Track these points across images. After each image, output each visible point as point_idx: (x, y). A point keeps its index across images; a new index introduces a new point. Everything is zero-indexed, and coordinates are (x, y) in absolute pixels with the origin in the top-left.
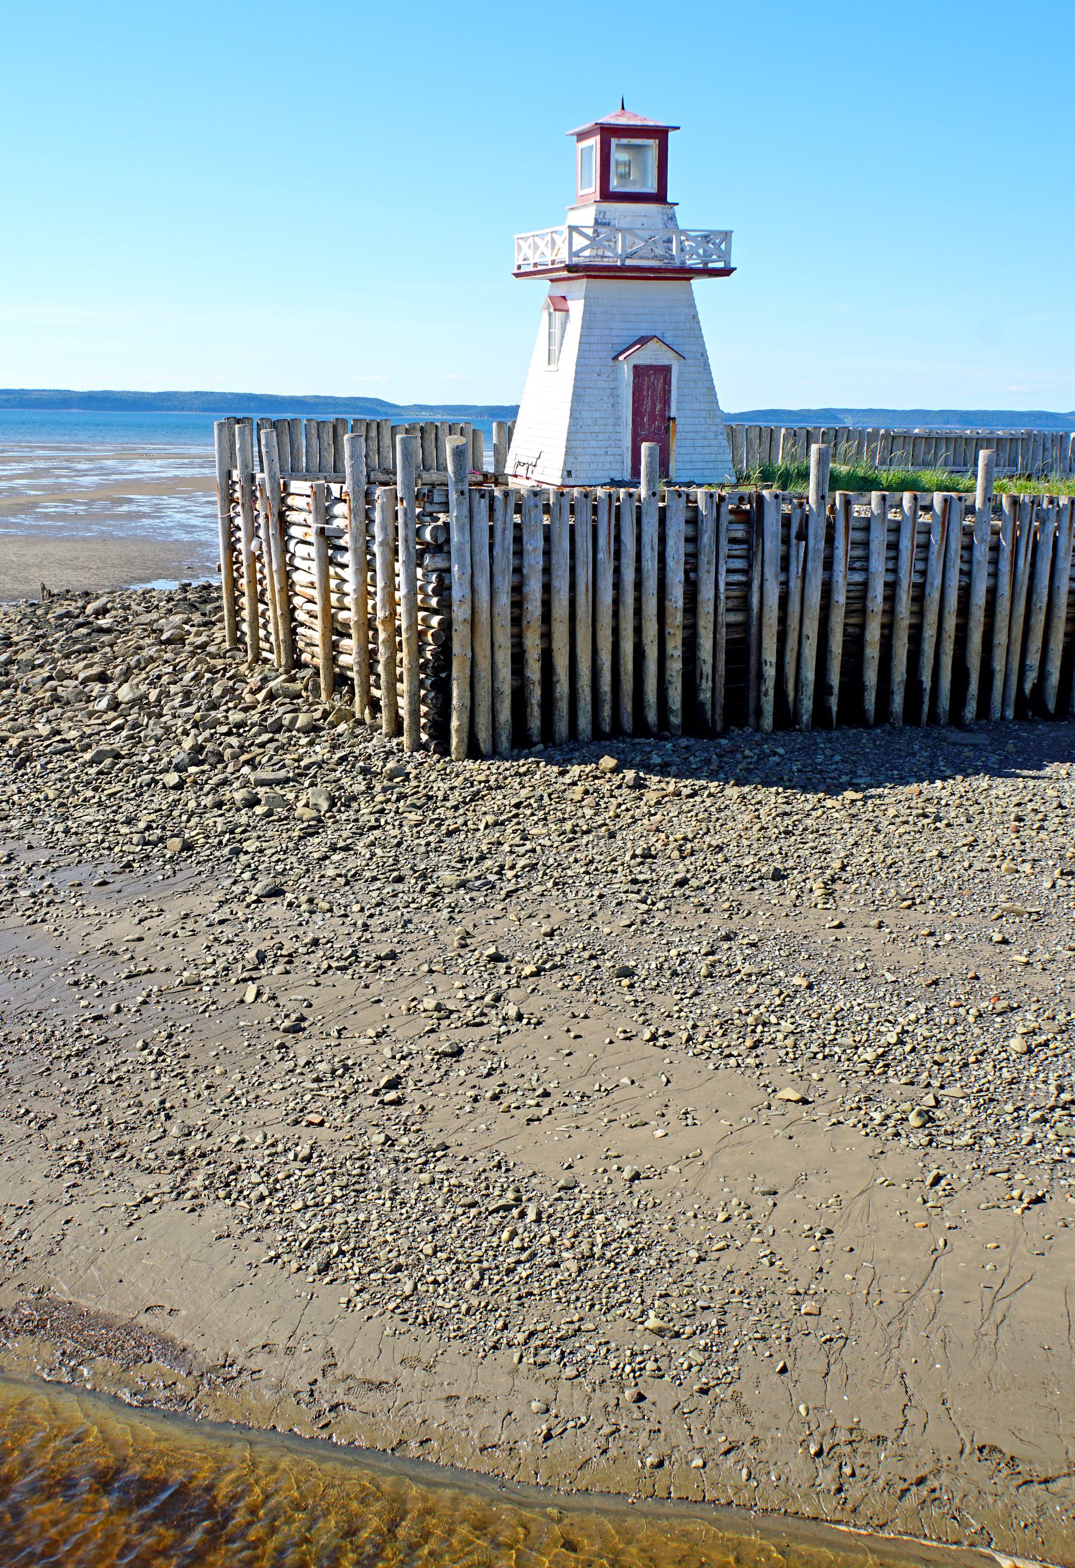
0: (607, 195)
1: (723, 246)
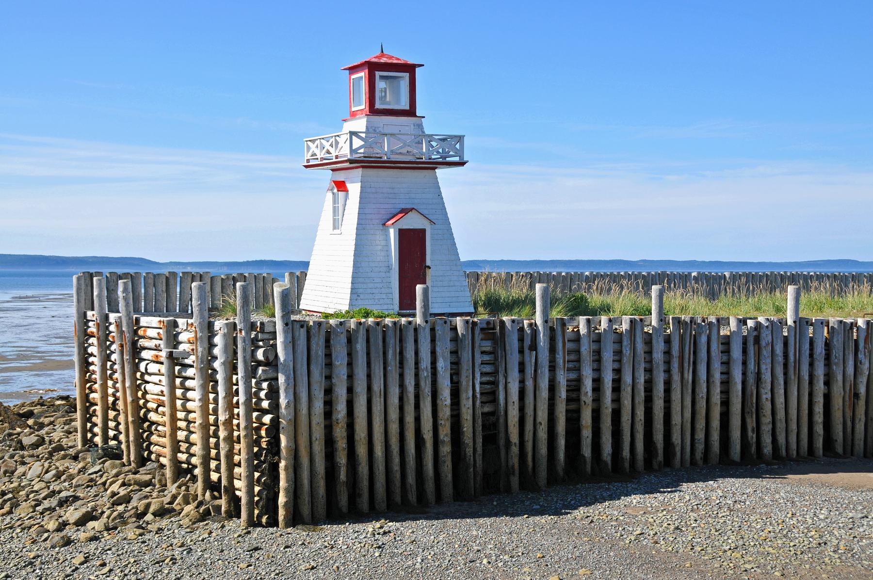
0: (373, 111)
1: (458, 146)
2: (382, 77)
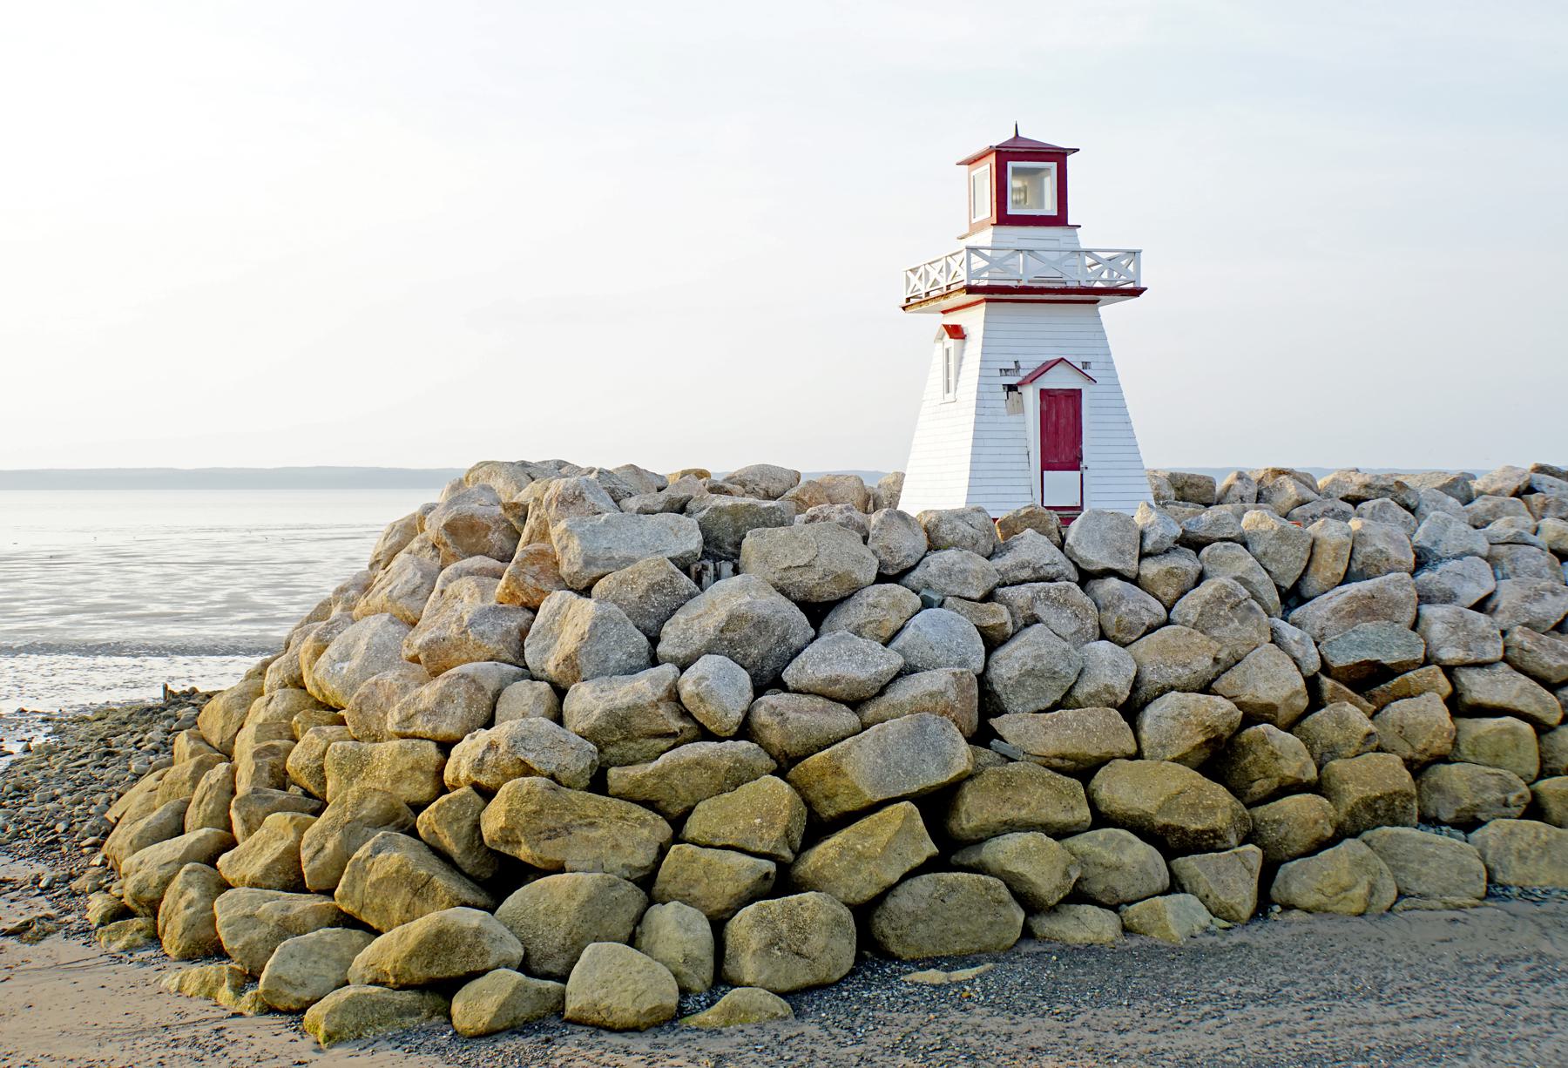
2: (1016, 171)
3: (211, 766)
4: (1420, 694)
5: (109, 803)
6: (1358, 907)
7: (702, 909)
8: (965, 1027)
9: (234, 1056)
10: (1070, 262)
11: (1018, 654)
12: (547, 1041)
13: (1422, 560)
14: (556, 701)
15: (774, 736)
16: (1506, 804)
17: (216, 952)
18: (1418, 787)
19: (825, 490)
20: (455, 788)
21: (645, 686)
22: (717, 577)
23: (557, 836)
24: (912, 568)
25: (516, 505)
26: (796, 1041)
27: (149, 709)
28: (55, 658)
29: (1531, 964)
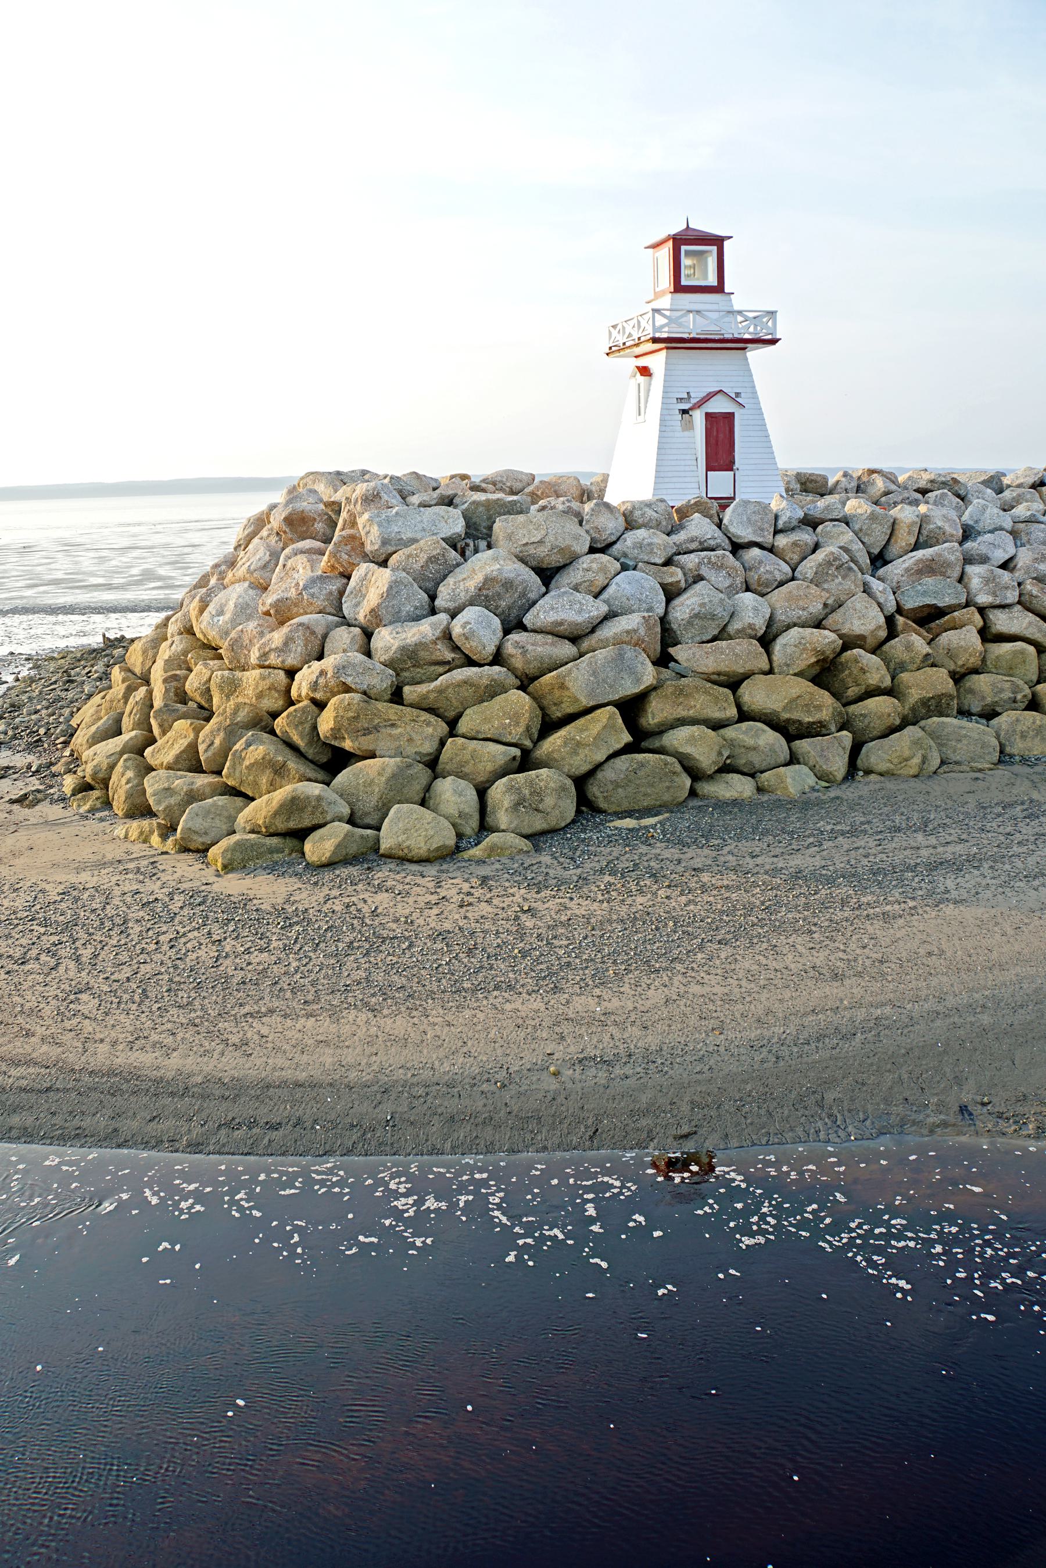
0: (679, 288)
1: (770, 324)
2: (688, 254)
3: (136, 689)
4: (962, 627)
5: (72, 714)
6: (913, 771)
7: (470, 781)
8: (649, 856)
9: (164, 879)
10: (726, 319)
11: (688, 602)
12: (369, 868)
13: (968, 533)
14: (366, 640)
15: (518, 663)
16: (1015, 701)
17: (148, 812)
18: (958, 691)
19: (553, 488)
20: (299, 702)
21: (426, 629)
22: (476, 551)
23: (370, 733)
24: (614, 543)
25: (333, 503)
26: (535, 867)
27: (94, 650)
28: (31, 617)
29: (1025, 807)
